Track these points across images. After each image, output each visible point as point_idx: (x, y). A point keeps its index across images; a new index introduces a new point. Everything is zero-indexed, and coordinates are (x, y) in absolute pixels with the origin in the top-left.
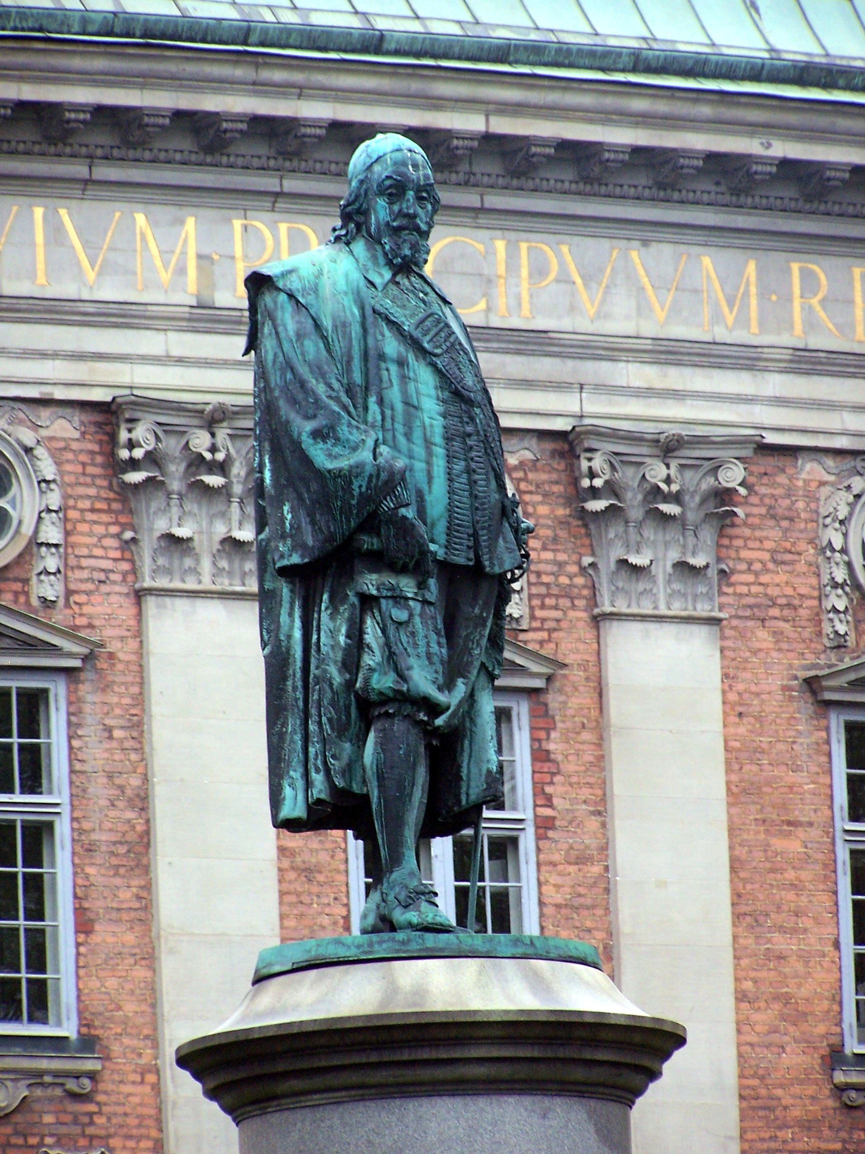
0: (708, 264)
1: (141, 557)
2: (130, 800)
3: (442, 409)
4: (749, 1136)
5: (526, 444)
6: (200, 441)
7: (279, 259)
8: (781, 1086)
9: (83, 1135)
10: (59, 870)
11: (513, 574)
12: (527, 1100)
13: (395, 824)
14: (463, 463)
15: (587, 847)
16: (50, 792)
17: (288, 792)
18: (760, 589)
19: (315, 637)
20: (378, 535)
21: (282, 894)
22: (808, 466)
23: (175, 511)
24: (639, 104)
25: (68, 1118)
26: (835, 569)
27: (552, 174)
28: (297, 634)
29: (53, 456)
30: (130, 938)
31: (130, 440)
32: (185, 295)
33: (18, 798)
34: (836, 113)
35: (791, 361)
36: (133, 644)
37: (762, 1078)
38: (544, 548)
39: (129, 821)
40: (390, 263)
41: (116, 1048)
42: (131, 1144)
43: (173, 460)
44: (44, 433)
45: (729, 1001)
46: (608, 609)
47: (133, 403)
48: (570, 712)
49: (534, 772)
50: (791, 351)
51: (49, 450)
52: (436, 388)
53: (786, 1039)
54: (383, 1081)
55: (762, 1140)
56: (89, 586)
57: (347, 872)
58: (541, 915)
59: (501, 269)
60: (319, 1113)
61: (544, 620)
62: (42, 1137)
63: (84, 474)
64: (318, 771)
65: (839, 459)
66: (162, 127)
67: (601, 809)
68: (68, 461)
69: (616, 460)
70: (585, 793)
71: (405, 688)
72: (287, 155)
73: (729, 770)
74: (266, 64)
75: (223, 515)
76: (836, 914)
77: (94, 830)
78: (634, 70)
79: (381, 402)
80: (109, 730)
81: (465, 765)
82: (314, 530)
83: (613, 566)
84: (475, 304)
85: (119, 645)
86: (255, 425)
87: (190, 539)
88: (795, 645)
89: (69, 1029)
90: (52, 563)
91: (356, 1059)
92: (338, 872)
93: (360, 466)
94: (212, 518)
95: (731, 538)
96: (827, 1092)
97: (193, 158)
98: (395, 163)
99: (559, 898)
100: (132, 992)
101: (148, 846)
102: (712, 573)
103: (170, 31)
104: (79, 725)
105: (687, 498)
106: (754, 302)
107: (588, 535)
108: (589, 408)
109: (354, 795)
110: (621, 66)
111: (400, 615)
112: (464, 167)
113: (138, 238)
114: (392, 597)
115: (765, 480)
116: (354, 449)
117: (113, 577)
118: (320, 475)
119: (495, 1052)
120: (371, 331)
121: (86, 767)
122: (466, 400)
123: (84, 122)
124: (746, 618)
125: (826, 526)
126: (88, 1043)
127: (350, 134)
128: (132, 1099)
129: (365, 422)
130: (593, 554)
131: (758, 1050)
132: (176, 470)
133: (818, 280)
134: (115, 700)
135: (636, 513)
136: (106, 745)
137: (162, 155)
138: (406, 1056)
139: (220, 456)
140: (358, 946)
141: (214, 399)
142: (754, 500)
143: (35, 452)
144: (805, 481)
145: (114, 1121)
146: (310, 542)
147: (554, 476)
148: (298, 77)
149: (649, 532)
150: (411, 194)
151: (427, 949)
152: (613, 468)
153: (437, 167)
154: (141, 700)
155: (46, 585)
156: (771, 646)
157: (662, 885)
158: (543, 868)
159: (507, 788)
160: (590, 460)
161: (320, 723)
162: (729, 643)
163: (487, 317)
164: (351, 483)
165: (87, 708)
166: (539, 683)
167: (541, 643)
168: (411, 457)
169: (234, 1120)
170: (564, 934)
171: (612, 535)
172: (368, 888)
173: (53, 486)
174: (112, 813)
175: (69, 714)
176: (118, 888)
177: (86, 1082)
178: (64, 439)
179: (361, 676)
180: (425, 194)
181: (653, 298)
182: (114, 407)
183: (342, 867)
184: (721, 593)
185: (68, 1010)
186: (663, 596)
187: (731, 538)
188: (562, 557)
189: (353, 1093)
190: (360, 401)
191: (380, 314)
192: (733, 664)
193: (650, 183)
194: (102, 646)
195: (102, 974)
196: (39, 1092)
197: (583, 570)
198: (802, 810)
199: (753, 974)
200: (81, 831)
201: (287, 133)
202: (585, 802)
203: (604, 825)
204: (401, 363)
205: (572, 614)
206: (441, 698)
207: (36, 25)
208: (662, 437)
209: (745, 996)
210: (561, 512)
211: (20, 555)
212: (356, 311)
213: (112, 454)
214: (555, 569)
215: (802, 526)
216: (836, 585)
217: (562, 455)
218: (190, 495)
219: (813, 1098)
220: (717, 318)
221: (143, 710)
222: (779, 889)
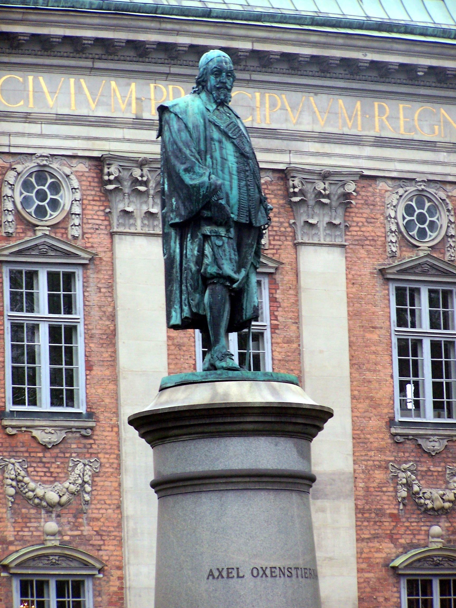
0: (341, 102)
1: (113, 220)
2: (108, 317)
3: (235, 160)
4: (357, 454)
5: (268, 174)
6: (137, 173)
7: (169, 100)
8: (370, 434)
9: (88, 452)
10: (79, 345)
11: (264, 227)
12: (269, 439)
13: (217, 326)
14: (244, 182)
15: (292, 337)
16: (76, 314)
17: (174, 314)
18: (361, 233)
19: (185, 251)
20: (211, 211)
21: (169, 355)
22: (381, 184)
23: (127, 201)
24: (314, 38)
25: (81, 446)
26: (391, 225)
27: (279, 66)
28: (178, 250)
29: (78, 179)
30: (108, 372)
31: (108, 172)
32: (131, 114)
33: (62, 316)
34: (392, 42)
35: (375, 142)
36: (109, 254)
37: (362, 431)
38: (275, 216)
39: (108, 325)
40: (215, 102)
41: (101, 417)
42: (107, 456)
43: (126, 180)
44: (74, 169)
45: (348, 399)
46: (300, 241)
47: (110, 157)
48: (285, 282)
49: (270, 306)
50: (55, 115)
51: (76, 176)
52: (234, 152)
53: (372, 414)
54: (212, 431)
55: (362, 456)
56: (92, 231)
57: (195, 346)
58: (273, 364)
59: (258, 104)
60: (186, 443)
61: (274, 245)
62: (71, 453)
63: (90, 186)
64: (186, 305)
65: (393, 181)
66: (122, 47)
67: (297, 321)
68: (84, 181)
69: (304, 181)
70: (291, 315)
71: (221, 272)
72: (172, 58)
73: (348, 306)
74: (164, 22)
75: (146, 202)
76: (392, 364)
77: (93, 329)
78: (312, 25)
79: (212, 157)
80: (99, 288)
81: (245, 303)
82: (184, 208)
83: (302, 224)
84: (248, 118)
85: (104, 254)
86: (162, 166)
87: (132, 212)
88: (375, 256)
89: (82, 409)
90: (77, 222)
91: (203, 421)
92: (191, 346)
93: (203, 183)
94: (141, 204)
95: (350, 212)
96: (388, 436)
97: (135, 59)
98: (218, 62)
99: (280, 357)
100: (108, 394)
101: (115, 335)
102: (342, 227)
103: (125, 8)
104: (87, 287)
105: (332, 196)
106: (359, 118)
107: (293, 211)
108: (293, 160)
109: (200, 315)
110: (306, 23)
111: (219, 243)
112: (243, 63)
113: (112, 91)
114: (216, 236)
115: (364, 189)
116: (201, 176)
117: (101, 227)
118: (187, 186)
119: (257, 419)
120: (208, 129)
121: (91, 304)
122: (246, 157)
123: (90, 44)
124: (356, 245)
125: (388, 208)
126: (90, 415)
127: (199, 50)
128: (107, 438)
129: (205, 165)
130: (294, 219)
131: (360, 419)
132: (127, 184)
133: (385, 109)
134: (102, 276)
135: (311, 203)
136: (99, 294)
137: (122, 58)
138: (221, 420)
139: (145, 179)
140: (202, 376)
141: (143, 156)
142: (359, 197)
143: (71, 177)
144: (380, 190)
145: (100, 447)
146: (183, 213)
147: (279, 188)
148: (177, 27)
149: (317, 210)
150: (224, 74)
151: (230, 377)
152: (303, 184)
153: (234, 63)
154: (112, 276)
155: (74, 230)
156: (366, 256)
157: (321, 352)
158: (274, 345)
159: (260, 312)
160: (293, 181)
161: (187, 287)
162: (349, 255)
163: (252, 123)
164: (200, 190)
165: (91, 280)
166: (272, 271)
167: (273, 254)
168: (224, 179)
169: (151, 446)
170: (282, 371)
171: (302, 211)
172: (204, 354)
173: (77, 190)
174: (100, 322)
175: (84, 282)
176: (103, 352)
177: (89, 431)
178: (82, 172)
179: (203, 267)
180: (230, 74)
181: (319, 117)
182: (102, 159)
183: (193, 344)
184: (346, 235)
185: (82, 402)
186: (322, 236)
187: (350, 212)
188: (282, 220)
189: (199, 435)
190: (203, 157)
191: (211, 122)
192: (350, 263)
193: (318, 70)
194: (97, 255)
195: (96, 387)
196: (70, 435)
197: (290, 225)
198: (378, 323)
199: (358, 388)
200: (88, 329)
201: (172, 49)
202: (291, 318)
203: (298, 328)
204: (220, 142)
205: (286, 243)
206: (235, 276)
207: (71, 5)
208: (322, 172)
209: (355, 397)
210: (282, 202)
211: (64, 218)
212: (202, 121)
213: (101, 178)
214: (279, 225)
215: (379, 208)
216: (392, 232)
217: (282, 179)
218: (133, 195)
219: (382, 439)
220: (345, 124)
221: (113, 281)
222: (368, 353)
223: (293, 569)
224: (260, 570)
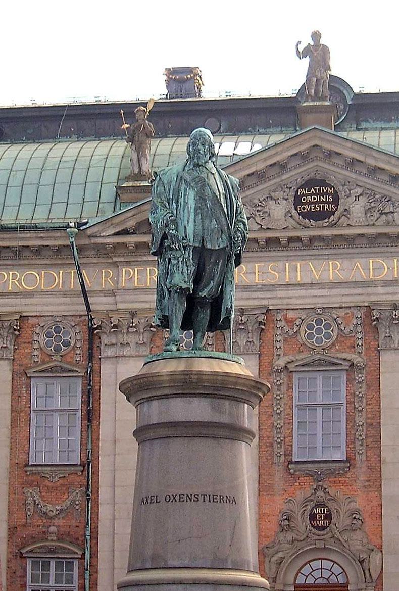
223: (200, 495)
224: (171, 496)
